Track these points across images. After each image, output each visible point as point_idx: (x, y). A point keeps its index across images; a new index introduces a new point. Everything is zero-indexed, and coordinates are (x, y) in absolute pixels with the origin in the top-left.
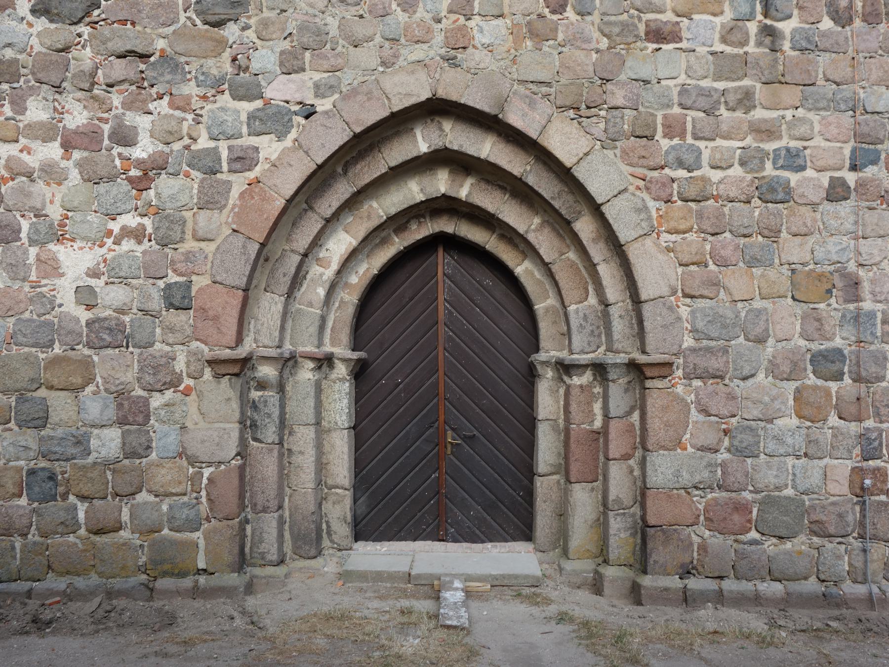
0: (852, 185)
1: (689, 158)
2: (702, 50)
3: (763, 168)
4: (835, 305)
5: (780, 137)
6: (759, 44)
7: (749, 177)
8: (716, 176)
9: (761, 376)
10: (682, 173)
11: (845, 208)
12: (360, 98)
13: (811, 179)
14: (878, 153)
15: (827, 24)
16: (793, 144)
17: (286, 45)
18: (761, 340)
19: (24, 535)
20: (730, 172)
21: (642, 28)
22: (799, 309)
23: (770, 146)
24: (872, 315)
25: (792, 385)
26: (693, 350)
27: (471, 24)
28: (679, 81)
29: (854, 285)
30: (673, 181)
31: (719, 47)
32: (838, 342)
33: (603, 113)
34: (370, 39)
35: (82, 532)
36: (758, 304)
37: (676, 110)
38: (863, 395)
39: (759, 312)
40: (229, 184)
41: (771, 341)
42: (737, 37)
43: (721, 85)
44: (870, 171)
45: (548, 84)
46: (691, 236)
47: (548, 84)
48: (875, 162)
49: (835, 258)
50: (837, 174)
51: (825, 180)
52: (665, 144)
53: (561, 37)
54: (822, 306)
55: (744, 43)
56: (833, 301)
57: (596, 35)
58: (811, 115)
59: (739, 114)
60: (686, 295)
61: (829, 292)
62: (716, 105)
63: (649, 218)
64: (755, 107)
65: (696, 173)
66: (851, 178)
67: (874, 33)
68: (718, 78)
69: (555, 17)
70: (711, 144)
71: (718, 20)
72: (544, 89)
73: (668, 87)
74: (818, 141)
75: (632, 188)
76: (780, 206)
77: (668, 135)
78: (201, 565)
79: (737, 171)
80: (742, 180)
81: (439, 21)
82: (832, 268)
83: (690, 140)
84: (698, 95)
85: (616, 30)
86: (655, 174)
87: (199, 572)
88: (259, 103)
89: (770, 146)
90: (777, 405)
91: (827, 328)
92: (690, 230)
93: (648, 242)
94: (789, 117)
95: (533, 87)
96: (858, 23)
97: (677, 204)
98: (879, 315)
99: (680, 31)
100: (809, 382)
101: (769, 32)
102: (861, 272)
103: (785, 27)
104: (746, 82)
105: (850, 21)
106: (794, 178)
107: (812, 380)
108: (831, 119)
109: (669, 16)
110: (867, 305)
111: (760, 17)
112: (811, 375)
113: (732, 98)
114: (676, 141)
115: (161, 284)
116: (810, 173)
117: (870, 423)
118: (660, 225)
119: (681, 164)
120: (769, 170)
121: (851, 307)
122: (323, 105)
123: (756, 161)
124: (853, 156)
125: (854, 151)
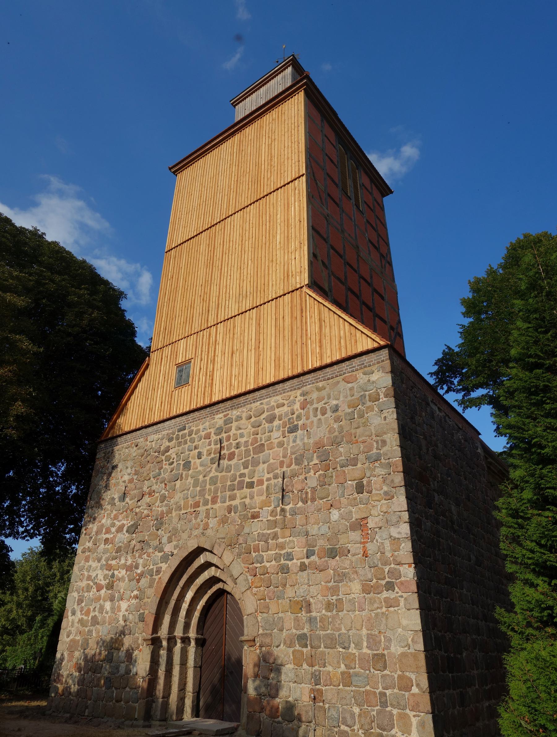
0: (307, 564)
1: (260, 559)
2: (265, 520)
3: (280, 561)
4: (304, 615)
5: (285, 548)
6: (280, 515)
7: (277, 564)
8: (268, 565)
9: (282, 645)
10: (259, 565)
11: (305, 574)
12: (183, 549)
13: (295, 563)
14: (314, 551)
15: (300, 504)
16: (289, 550)
17: (169, 534)
18: (281, 630)
19: (102, 701)
20: (272, 563)
21: (250, 515)
22: (293, 616)
23: (283, 552)
24: (316, 618)
25: (291, 650)
26: (262, 635)
27: (209, 521)
28: (258, 532)
29: (309, 605)
30: (257, 568)
31: (270, 518)
32: (305, 631)
33: (237, 546)
34: (186, 530)
35: (114, 701)
36: (280, 615)
37: (257, 542)
38: (313, 654)
39: (281, 618)
40: (155, 579)
41: (285, 630)
42: (274, 514)
43: (269, 532)
44: (313, 558)
45: (224, 538)
46: (262, 588)
47: (224, 538)
48: (313, 555)
49: (303, 595)
50: (303, 561)
51: (299, 563)
52: (254, 554)
53: (229, 522)
54: (300, 615)
55: (276, 515)
56: (303, 612)
57: (238, 519)
58: (295, 539)
59: (274, 541)
60: (260, 612)
61: (301, 609)
62: (268, 538)
63: (249, 583)
64: (278, 538)
65: (263, 564)
66: (306, 561)
67: (313, 505)
68: (268, 530)
69: (229, 515)
70: (266, 553)
71: (269, 508)
72: (223, 540)
73: (255, 535)
74: (296, 549)
75: (244, 572)
76: (287, 575)
77: (255, 552)
78: (136, 717)
79: (274, 563)
80: (275, 565)
81: (202, 521)
82: (302, 599)
83: (261, 553)
84: (262, 536)
85: (242, 517)
86: (251, 566)
87: (136, 719)
88: (163, 553)
89: (283, 552)
90: (286, 659)
91: (301, 624)
92: (261, 586)
93: (248, 592)
94: (288, 541)
95: (221, 540)
96: (309, 502)
97: (102, 595)
98: (318, 618)
99: (92, 471)
100: (297, 648)
101: (283, 510)
102: (311, 600)
103: (288, 508)
104: (276, 529)
105: (307, 502)
106: (290, 563)
107: (298, 647)
108: (299, 540)
109: (257, 510)
110: (314, 614)
111: (281, 505)
112: (297, 645)
113: (271, 536)
114: (257, 553)
115: (139, 613)
116: (295, 561)
117: (316, 668)
118: (252, 585)
119: (258, 562)
120: (283, 562)
121: (308, 615)
122: (175, 552)
123: (278, 558)
124: (307, 553)
125: (307, 550)
